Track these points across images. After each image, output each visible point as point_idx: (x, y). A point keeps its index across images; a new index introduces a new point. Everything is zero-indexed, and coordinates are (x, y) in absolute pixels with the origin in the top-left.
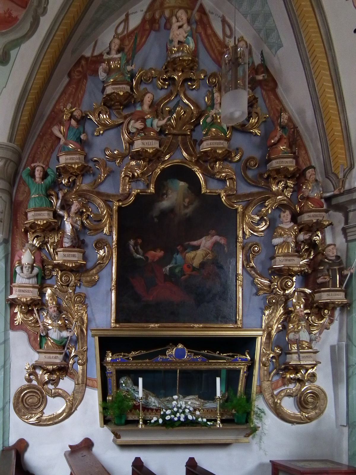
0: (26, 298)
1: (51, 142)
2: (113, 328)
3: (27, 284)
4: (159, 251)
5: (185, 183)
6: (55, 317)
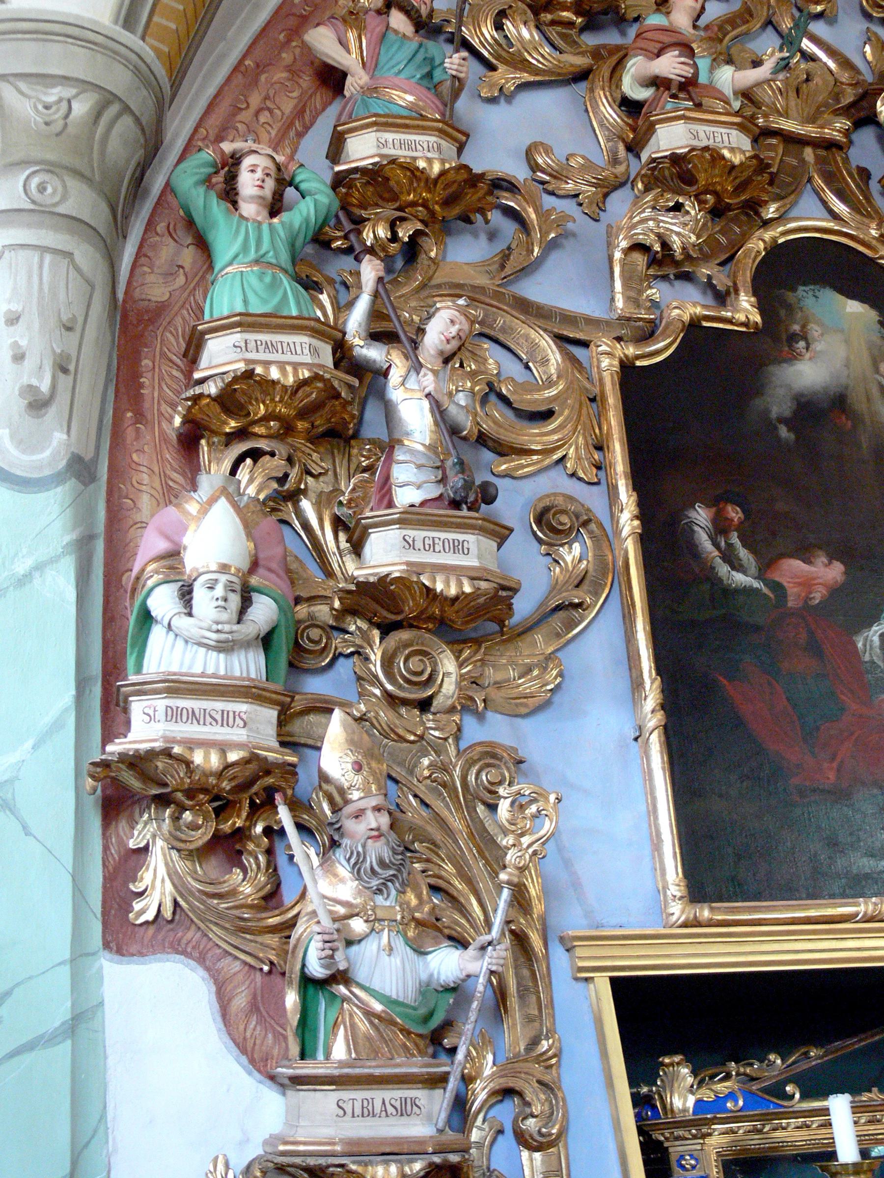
0: (223, 753)
1: (295, 94)
2: (685, 925)
3: (214, 676)
4: (825, 560)
5: (866, 306)
6: (382, 863)
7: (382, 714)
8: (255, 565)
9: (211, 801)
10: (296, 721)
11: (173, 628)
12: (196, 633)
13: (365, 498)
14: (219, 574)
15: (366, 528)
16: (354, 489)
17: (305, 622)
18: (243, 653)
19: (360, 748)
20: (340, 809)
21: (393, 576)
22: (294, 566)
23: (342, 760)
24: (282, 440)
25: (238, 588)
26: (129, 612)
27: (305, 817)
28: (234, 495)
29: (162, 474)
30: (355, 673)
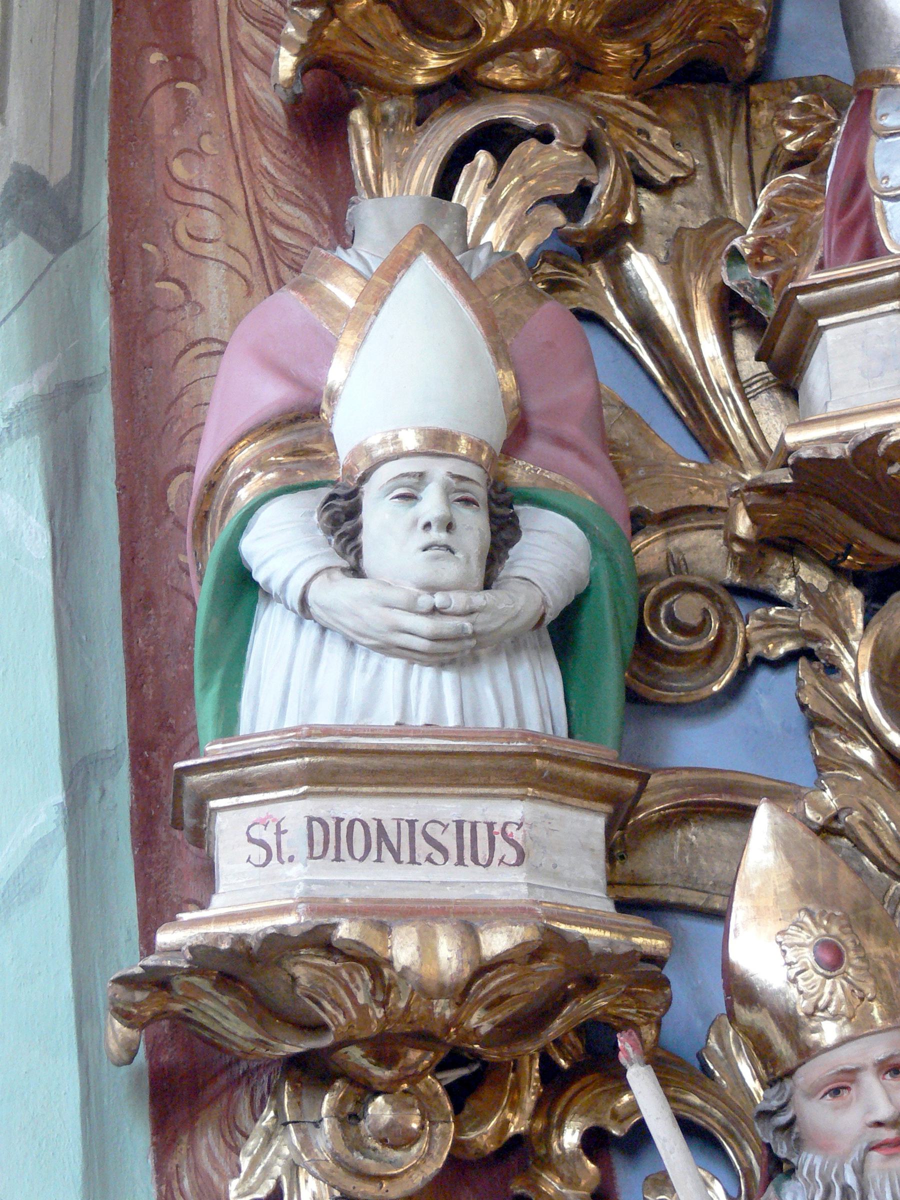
3: (431, 730)
7: (882, 813)
8: (519, 432)
9: (442, 1067)
10: (659, 838)
11: (315, 610)
13: (801, 237)
15: (811, 315)
16: (768, 217)
17: (660, 577)
18: (502, 669)
19: (835, 904)
20: (790, 1074)
21: (893, 439)
22: (621, 432)
23: (787, 940)
24: (567, 97)
25: (480, 493)
26: (194, 577)
28: (454, 249)
29: (254, 209)
30: (803, 707)
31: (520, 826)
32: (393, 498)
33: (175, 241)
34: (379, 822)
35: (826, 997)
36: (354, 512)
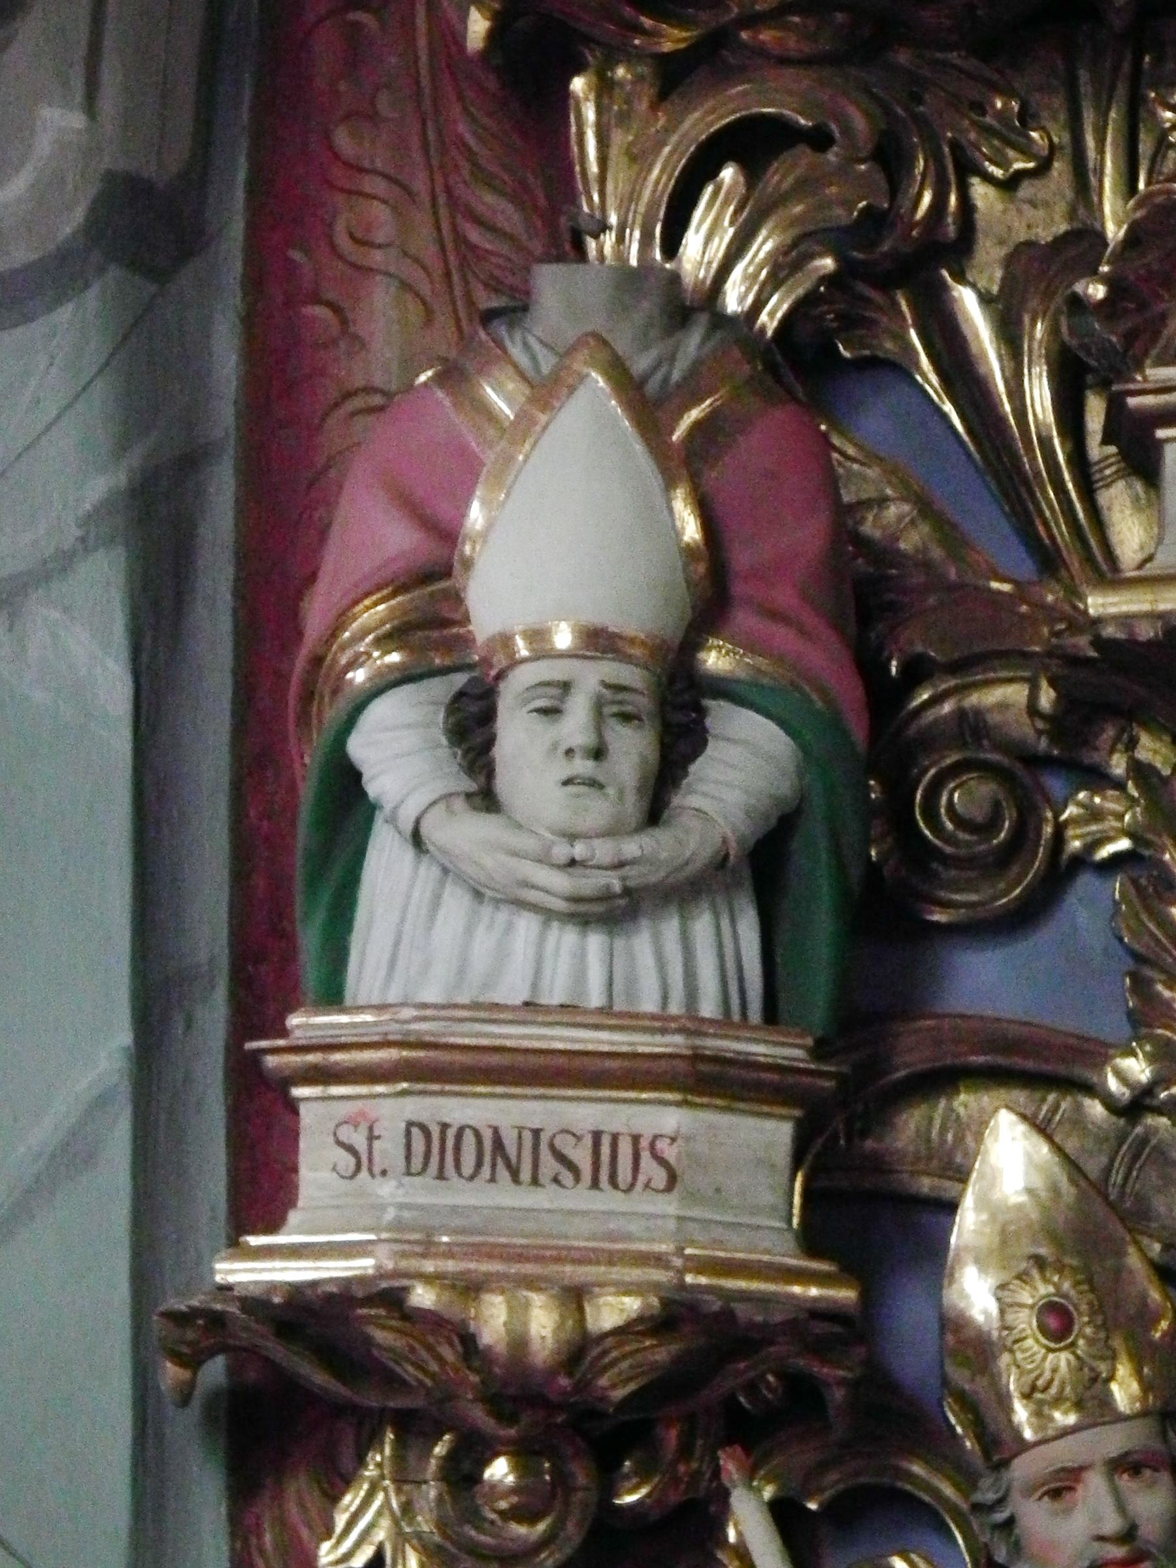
0: (575, 1297)
3: (570, 1012)
12: (495, 866)
14: (576, 663)
18: (671, 927)
25: (643, 703)
27: (917, 1469)
29: (442, 200)
31: (673, 1140)
32: (531, 711)
33: (333, 247)
34: (496, 1131)
35: (1047, 1375)
36: (488, 716)
